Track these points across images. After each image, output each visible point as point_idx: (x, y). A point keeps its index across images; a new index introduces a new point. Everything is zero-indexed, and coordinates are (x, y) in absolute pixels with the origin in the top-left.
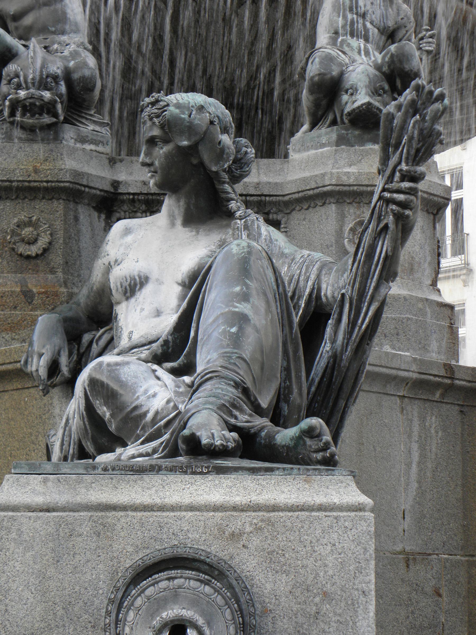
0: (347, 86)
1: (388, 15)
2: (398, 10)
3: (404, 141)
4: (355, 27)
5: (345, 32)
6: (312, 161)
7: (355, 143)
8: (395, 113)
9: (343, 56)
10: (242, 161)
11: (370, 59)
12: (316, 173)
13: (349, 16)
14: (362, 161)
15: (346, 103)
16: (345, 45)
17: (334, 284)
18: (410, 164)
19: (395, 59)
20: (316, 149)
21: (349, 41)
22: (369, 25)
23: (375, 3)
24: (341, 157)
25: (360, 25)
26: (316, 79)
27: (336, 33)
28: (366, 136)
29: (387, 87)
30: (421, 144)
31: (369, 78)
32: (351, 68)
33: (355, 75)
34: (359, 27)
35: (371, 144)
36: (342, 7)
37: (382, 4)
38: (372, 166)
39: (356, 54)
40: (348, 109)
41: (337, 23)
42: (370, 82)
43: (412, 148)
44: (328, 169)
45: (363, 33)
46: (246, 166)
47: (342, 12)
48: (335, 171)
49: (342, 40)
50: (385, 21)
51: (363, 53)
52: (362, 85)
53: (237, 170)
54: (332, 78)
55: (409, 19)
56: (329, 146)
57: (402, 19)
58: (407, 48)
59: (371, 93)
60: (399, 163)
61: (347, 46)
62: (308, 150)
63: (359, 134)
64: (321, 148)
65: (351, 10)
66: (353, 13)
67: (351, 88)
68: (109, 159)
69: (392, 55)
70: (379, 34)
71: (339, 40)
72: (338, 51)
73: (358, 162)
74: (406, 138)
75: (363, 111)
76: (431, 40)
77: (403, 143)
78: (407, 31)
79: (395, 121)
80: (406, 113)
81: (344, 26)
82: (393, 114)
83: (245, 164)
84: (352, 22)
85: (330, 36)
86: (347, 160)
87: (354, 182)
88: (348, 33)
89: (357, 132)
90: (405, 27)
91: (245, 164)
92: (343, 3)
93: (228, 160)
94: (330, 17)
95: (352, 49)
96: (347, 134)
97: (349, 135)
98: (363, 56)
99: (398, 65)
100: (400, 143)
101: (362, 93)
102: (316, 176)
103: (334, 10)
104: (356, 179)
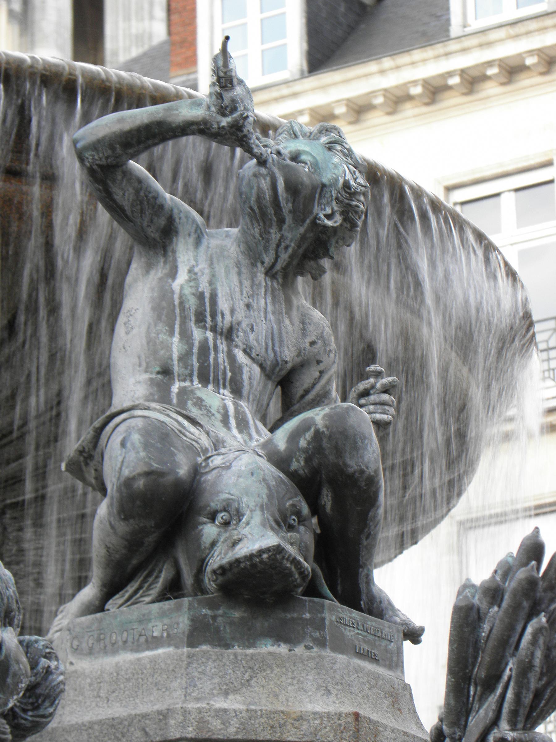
0: (214, 505)
1: (284, 335)
2: (303, 322)
3: (507, 672)
4: (211, 360)
5: (187, 372)
6: (128, 680)
7: (233, 639)
8: (484, 606)
9: (192, 429)
10: (39, 691)
11: (251, 437)
12: (143, 709)
13: (197, 334)
14: (253, 682)
15: (213, 544)
16: (190, 403)
18: (520, 726)
19: (325, 444)
20: (137, 649)
21: (199, 394)
22: (241, 357)
23: (255, 305)
24: (203, 673)
25: (222, 357)
26: (141, 483)
27: (166, 372)
28: (260, 624)
29: (305, 510)
30: (545, 679)
31: (269, 488)
32: (217, 461)
33: (233, 479)
34: (220, 360)
35: (270, 642)
36: (177, 311)
37: (270, 308)
38: (276, 696)
39: (219, 425)
40: (218, 558)
41: (169, 348)
42: (270, 496)
43: (528, 689)
44: (174, 698)
45: (229, 374)
46: (47, 704)
47: (178, 323)
48: (191, 706)
49: (183, 392)
50: (277, 348)
51: (233, 422)
52: (252, 504)
53: (25, 711)
54: (178, 483)
55: (326, 344)
56: (169, 645)
57: (312, 343)
58: (352, 420)
59: (273, 524)
60: (495, 722)
61: (195, 404)
62: (115, 652)
63: (242, 618)
64: (148, 649)
65: (200, 319)
66: (205, 328)
67: (225, 510)
69: (318, 434)
70: (263, 378)
71: (175, 388)
72: (180, 418)
73: (243, 685)
74: (510, 665)
75: (260, 567)
76: (386, 397)
77: (505, 678)
78: (321, 372)
79: (486, 627)
80: (515, 608)
81: (184, 358)
82: (479, 610)
83: (47, 697)
84: (204, 349)
85: (151, 380)
86: (217, 680)
87: (237, 733)
88: (196, 374)
89: (237, 614)
90: (319, 362)
91: (47, 697)
92: (181, 303)
93: (14, 691)
94: (148, 332)
95: (209, 414)
96: (214, 618)
97: (220, 619)
98: (235, 431)
99: (332, 458)
100: (499, 677)
101: (253, 522)
102: (145, 716)
103: (159, 318)
104: (243, 726)
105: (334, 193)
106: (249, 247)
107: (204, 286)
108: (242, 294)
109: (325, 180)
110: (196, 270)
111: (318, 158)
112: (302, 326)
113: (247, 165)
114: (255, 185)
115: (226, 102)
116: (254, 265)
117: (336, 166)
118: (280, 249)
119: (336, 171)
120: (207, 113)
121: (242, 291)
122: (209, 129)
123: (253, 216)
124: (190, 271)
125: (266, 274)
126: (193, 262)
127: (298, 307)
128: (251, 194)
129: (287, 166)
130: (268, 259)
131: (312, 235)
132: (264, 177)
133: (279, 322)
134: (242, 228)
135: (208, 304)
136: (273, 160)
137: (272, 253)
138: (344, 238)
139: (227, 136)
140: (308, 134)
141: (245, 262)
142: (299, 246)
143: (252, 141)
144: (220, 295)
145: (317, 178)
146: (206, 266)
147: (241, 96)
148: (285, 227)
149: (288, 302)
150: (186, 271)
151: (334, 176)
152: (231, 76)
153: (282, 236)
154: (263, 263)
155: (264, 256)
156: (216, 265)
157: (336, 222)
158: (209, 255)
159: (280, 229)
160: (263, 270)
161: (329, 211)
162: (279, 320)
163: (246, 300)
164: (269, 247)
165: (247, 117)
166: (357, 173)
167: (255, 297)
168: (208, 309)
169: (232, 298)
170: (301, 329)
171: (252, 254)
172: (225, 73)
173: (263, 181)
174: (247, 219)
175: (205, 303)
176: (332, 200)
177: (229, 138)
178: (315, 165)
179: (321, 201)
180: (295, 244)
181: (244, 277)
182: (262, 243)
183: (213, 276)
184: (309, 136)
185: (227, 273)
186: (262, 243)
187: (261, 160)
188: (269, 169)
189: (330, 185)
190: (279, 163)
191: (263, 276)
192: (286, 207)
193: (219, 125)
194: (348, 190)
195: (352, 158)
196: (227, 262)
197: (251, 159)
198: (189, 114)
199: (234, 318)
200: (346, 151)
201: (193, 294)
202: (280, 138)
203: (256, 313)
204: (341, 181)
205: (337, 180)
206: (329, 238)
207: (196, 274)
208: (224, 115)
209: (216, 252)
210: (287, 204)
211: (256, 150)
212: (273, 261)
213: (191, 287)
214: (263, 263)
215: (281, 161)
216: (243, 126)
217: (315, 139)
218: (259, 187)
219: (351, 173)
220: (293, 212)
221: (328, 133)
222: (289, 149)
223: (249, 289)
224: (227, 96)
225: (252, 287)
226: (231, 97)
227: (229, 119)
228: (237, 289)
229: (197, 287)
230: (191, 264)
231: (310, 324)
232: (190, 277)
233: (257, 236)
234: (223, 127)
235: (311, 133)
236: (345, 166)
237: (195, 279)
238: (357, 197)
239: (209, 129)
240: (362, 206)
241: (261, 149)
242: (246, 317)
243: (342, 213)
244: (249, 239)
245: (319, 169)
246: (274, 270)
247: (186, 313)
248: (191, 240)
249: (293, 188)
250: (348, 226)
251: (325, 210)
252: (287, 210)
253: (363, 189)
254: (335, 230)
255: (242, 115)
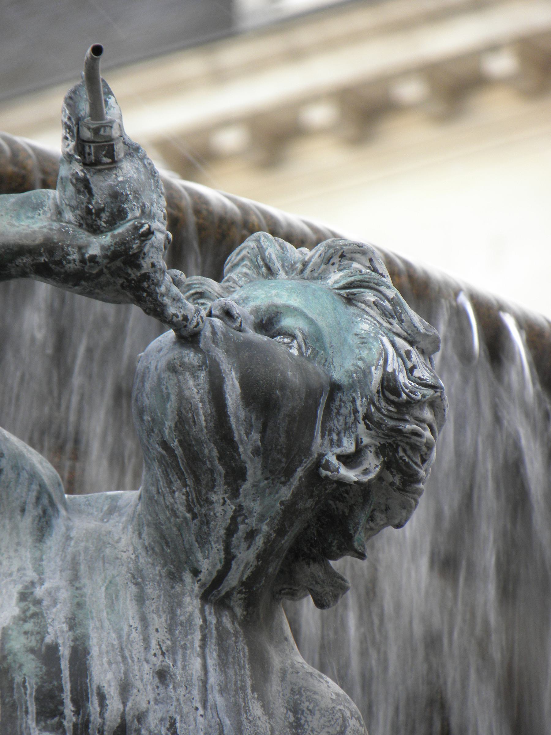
2: (295, 709)
17: (363, 273)
23: (178, 671)
68: (129, 201)
105: (361, 405)
106: (163, 537)
107: (57, 630)
108: (147, 648)
109: (338, 375)
110: (39, 592)
111: (321, 323)
112: (292, 719)
113: (154, 344)
114: (173, 392)
115: (100, 198)
116: (174, 577)
117: (364, 341)
118: (234, 540)
119: (364, 353)
120: (56, 225)
121: (146, 640)
122: (59, 263)
123: (168, 461)
124: (24, 597)
125: (205, 597)
126: (31, 575)
127: (284, 672)
128: (164, 414)
129: (249, 344)
130: (208, 563)
131: (310, 503)
132: (194, 371)
133: (238, 711)
134: (146, 490)
135: (66, 674)
136: (214, 333)
137: (217, 550)
138: (387, 509)
139: (103, 279)
140: (299, 266)
141: (154, 570)
142: (281, 532)
143: (163, 289)
144: (95, 651)
145: (320, 369)
146: (63, 583)
147: (135, 185)
148: (246, 486)
149: (260, 663)
150: (16, 596)
151: (360, 363)
152: (110, 139)
153: (240, 508)
154: (196, 572)
155: (200, 556)
156: (85, 581)
157: (366, 472)
158: (69, 558)
159: (235, 494)
160: (196, 587)
161: (349, 446)
162: (236, 704)
163: (157, 662)
164: (208, 534)
165: (150, 232)
166: (415, 354)
167: (180, 652)
168: (67, 686)
169: (124, 658)
170: (291, 726)
171: (171, 552)
172: (96, 131)
173: (191, 383)
174: (158, 471)
175: (60, 671)
176: (356, 420)
177: (108, 284)
178: (315, 341)
179: (330, 425)
180: (270, 525)
181: (151, 606)
182: (192, 526)
183: (79, 605)
184: (302, 271)
185: (112, 600)
186: (194, 525)
187: (185, 333)
188: (205, 353)
189: (352, 387)
190: (225, 335)
191: (197, 602)
192: (247, 440)
193: (83, 255)
194: (392, 398)
195: (401, 321)
196: (112, 571)
197: (161, 331)
198: (13, 230)
199: (129, 704)
200: (387, 304)
201: (32, 651)
202: (233, 275)
203: (181, 691)
204: (376, 375)
205: (366, 374)
206: (351, 509)
207: (38, 602)
208: (95, 230)
209: (86, 549)
210: (248, 434)
211: (172, 310)
212: (219, 567)
213: (26, 633)
214: (196, 572)
215: (233, 334)
216: (140, 254)
217: (314, 279)
218: (181, 395)
219: (399, 355)
220: (263, 452)
221: (345, 262)
222: (252, 304)
223: (163, 635)
224: (102, 185)
225: (171, 630)
226: (111, 186)
227: (106, 239)
228: (136, 636)
229: (42, 633)
230: (28, 579)
231: (312, 712)
232: (24, 611)
233: (182, 509)
234: (93, 258)
235: (305, 264)
236: (385, 340)
237: (35, 615)
238: (417, 412)
239: (59, 263)
240: (427, 434)
241: (184, 307)
242: (157, 702)
243: (380, 451)
244: (162, 517)
245: (325, 349)
246: (224, 589)
247: (16, 696)
248: (27, 523)
249: (262, 397)
250: (397, 480)
251: (339, 444)
252: (250, 448)
253: (430, 392)
254: (364, 490)
255: (136, 228)
